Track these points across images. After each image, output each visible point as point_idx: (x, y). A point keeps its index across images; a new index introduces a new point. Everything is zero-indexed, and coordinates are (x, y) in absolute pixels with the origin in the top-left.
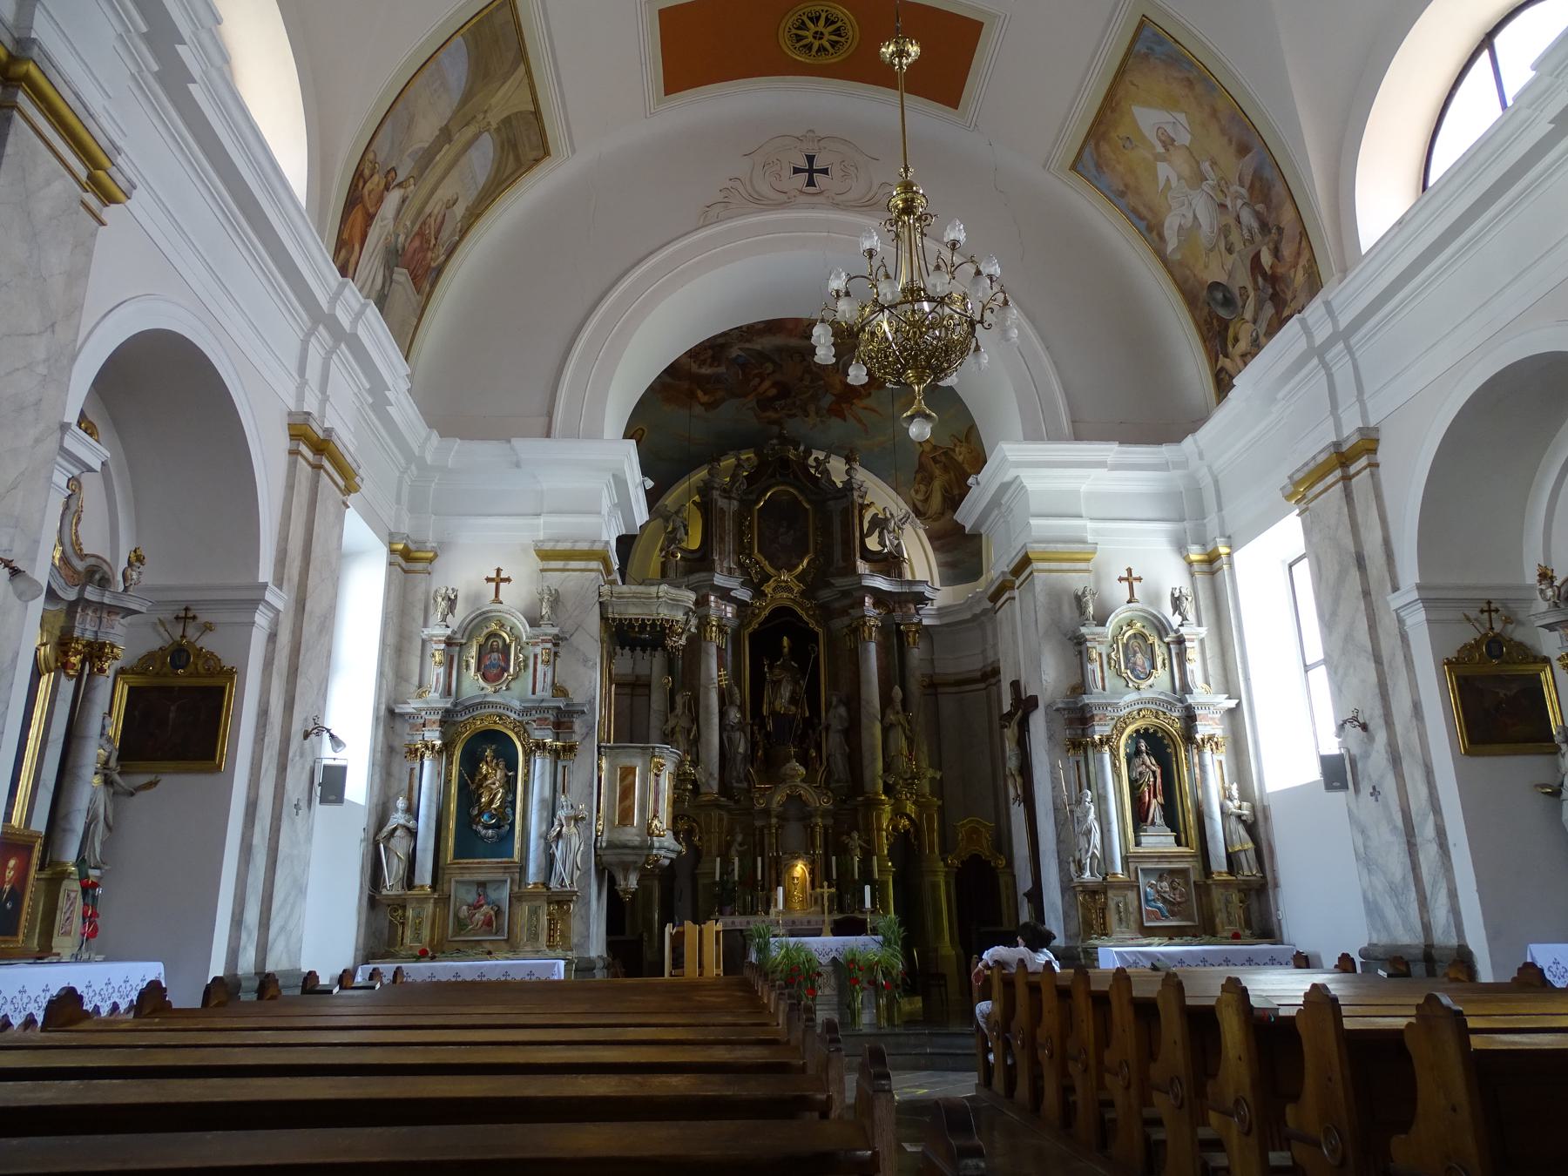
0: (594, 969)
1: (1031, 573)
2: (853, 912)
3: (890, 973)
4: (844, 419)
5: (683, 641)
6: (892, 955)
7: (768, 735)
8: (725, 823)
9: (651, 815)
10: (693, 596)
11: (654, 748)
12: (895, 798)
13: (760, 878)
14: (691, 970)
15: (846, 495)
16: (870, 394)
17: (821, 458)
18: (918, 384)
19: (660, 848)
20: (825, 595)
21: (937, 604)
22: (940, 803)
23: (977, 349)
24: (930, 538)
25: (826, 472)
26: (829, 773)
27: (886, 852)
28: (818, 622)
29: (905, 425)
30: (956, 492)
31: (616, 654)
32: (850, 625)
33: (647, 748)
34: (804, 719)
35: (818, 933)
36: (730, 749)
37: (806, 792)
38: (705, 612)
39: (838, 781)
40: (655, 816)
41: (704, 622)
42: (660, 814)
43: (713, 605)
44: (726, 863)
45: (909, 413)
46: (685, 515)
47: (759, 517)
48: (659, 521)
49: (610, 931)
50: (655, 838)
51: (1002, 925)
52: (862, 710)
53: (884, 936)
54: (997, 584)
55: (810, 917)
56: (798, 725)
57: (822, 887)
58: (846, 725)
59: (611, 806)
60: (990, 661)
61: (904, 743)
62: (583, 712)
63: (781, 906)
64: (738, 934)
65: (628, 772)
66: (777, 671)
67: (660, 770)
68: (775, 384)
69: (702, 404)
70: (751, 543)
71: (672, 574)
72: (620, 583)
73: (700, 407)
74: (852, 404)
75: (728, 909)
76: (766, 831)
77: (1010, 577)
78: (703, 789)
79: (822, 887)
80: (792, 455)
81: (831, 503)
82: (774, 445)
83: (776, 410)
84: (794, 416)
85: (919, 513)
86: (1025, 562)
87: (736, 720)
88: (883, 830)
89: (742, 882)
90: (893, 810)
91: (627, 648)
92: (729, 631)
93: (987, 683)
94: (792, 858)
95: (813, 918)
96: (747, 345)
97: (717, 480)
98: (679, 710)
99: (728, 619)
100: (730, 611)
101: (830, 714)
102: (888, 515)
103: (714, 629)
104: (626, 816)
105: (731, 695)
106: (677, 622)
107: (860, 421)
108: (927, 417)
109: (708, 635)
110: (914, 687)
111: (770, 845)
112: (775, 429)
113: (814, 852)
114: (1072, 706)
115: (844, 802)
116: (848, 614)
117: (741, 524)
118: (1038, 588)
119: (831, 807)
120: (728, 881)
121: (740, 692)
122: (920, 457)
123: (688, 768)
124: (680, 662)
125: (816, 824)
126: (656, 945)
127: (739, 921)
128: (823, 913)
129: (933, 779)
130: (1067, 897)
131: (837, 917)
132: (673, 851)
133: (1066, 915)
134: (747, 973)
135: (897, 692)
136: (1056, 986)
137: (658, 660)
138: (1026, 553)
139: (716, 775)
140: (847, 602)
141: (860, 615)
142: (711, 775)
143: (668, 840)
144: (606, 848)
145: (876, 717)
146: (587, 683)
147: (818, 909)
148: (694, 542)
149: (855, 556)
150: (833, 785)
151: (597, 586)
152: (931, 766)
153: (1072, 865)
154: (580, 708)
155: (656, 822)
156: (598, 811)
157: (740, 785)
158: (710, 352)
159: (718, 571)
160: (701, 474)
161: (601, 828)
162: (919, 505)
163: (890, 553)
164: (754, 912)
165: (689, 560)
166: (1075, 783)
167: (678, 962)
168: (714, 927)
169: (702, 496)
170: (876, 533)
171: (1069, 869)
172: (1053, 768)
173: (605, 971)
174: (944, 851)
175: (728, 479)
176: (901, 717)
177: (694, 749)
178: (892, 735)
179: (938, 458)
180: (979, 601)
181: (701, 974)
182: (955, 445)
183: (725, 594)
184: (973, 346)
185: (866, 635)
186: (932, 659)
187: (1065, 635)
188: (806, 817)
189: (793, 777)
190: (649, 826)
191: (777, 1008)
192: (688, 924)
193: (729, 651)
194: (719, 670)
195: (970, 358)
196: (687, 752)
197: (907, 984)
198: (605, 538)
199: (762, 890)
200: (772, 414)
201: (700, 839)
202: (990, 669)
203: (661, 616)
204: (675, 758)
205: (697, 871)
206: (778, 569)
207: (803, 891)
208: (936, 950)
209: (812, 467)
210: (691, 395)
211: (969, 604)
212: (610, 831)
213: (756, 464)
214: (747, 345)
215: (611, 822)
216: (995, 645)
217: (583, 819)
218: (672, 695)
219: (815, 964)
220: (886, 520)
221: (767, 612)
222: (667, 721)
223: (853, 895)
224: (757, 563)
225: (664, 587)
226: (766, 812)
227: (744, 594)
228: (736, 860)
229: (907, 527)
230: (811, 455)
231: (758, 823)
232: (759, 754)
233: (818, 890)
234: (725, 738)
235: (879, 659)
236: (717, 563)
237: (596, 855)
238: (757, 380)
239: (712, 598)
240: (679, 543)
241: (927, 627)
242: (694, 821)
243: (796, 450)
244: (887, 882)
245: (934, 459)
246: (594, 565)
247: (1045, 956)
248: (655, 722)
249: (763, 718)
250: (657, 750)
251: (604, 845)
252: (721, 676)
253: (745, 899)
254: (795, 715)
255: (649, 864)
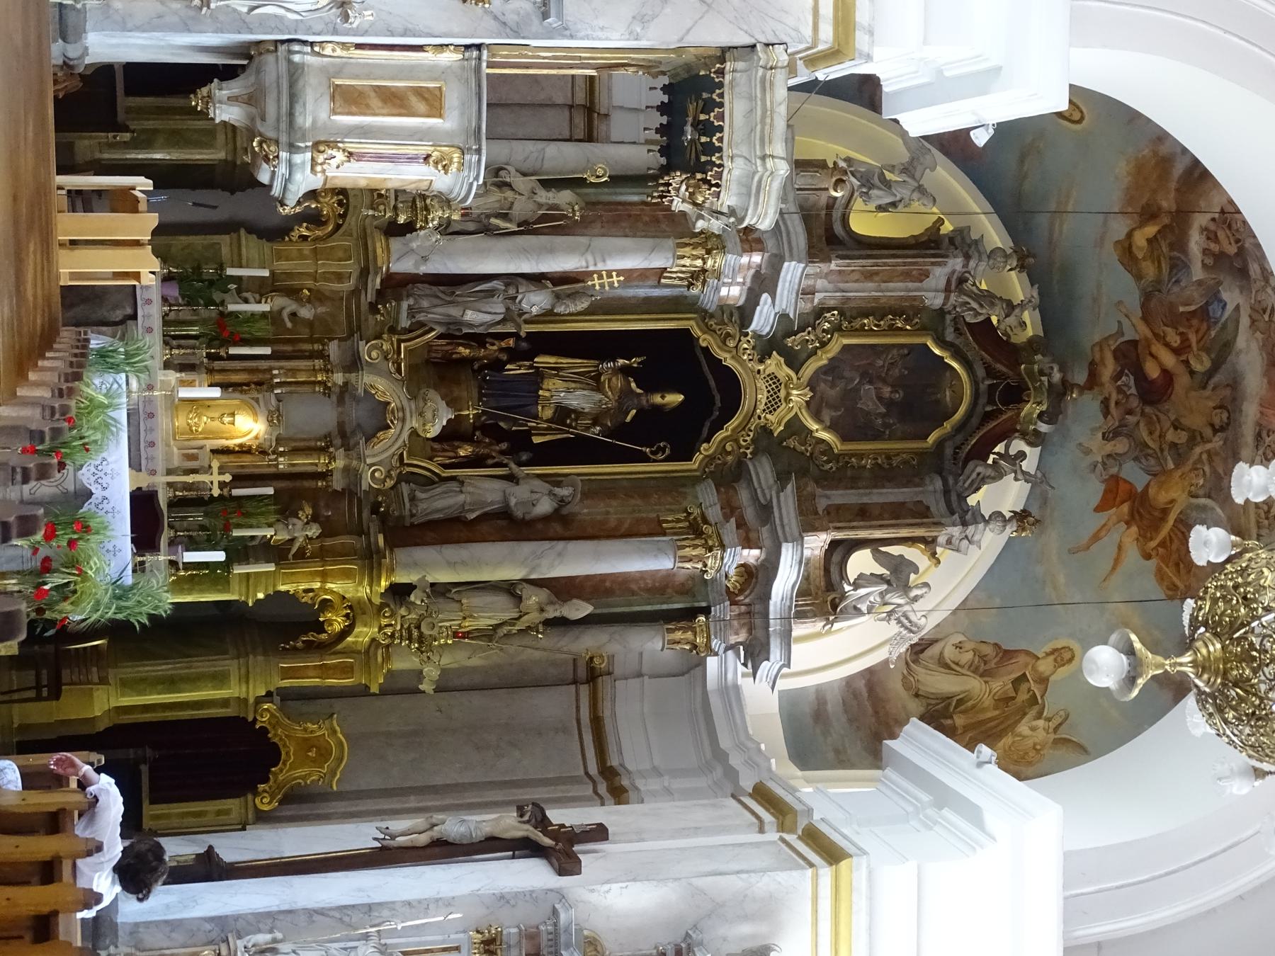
0: (64, 40)
1: (811, 865)
2: (171, 526)
3: (65, 599)
4: (1099, 509)
5: (678, 205)
6: (98, 603)
7: (497, 365)
8: (336, 286)
9: (352, 147)
10: (765, 224)
11: (479, 151)
12: (382, 606)
13: (233, 351)
14: (69, 225)
15: (952, 513)
16: (1147, 557)
17: (1025, 465)
18: (1194, 663)
19: (291, 165)
20: (763, 472)
21: (746, 684)
22: (374, 689)
23: (1259, 774)
24: (870, 672)
25: (998, 474)
26: (428, 482)
27: (283, 588)
28: (711, 458)
29: (1114, 637)
30: (959, 721)
31: (655, 76)
32: (706, 521)
33: (478, 140)
34: (528, 434)
35: (135, 464)
36: (470, 295)
37: (390, 443)
38: (729, 245)
39: (413, 499)
40: (351, 154)
41: (711, 243)
42: (354, 165)
43: (745, 260)
44: (263, 288)
45: (1138, 645)
46: (916, 206)
47: (911, 347)
48: (904, 156)
49: (132, 69)
50: (308, 155)
51: (152, 802)
52: (547, 544)
53: (132, 588)
54: (789, 799)
55: (160, 445)
56: (515, 422)
57: (222, 471)
58: (519, 513)
59: (370, 71)
60: (640, 783)
61: (484, 622)
62: (545, 15)
63: (185, 393)
64: (129, 311)
65: (433, 102)
66: (618, 382)
67: (436, 163)
68: (1167, 375)
69: (1130, 235)
70: (861, 331)
71: (804, 180)
72: (792, 82)
73: (1125, 231)
74: (1127, 523)
75: (174, 291)
76: (318, 363)
77: (802, 824)
78: (396, 243)
79: (222, 471)
80: (1031, 409)
81: (939, 484)
82: (1049, 375)
83: (1117, 377)
84: (1106, 412)
85: (918, 650)
86: (832, 854)
87: (525, 306)
88: (324, 582)
89: (225, 317)
90: (359, 601)
91: (666, 99)
92: (695, 291)
93: (599, 779)
94: (270, 413)
95: (159, 452)
96: (1245, 321)
97: (983, 265)
98: (545, 196)
99: (717, 289)
100: (733, 292)
101: (537, 483)
102: (914, 593)
103: (699, 263)
104: (349, 99)
105: (572, 296)
106: (718, 195)
107: (1096, 537)
108: (1131, 680)
109: (687, 251)
110: (589, 642)
111: (294, 371)
112: (1080, 377)
113: (282, 454)
114: (563, 939)
115: (375, 509)
116: (727, 518)
117: (897, 312)
118: (783, 877)
119: (364, 487)
120: (227, 291)
121: (579, 314)
122: (1027, 653)
123: (437, 215)
124: (635, 198)
125: (333, 458)
126: (106, 156)
127: (151, 313)
128: (169, 472)
129: (419, 675)
130: (208, 926)
131: (163, 500)
132: (285, 189)
133: (174, 925)
134: (67, 335)
135: (579, 609)
136: (55, 914)
137: (643, 157)
138: (851, 856)
139: (424, 269)
140: (750, 514)
141: (726, 542)
142: (425, 259)
143: (305, 181)
144: (290, 62)
145: (533, 570)
146: (601, 22)
147: (176, 462)
148: (864, 223)
149: (838, 529)
150: (405, 489)
151: (785, 39)
152: (444, 672)
153: (268, 937)
154: (553, 11)
155: (340, 156)
156: (359, 46)
157: (404, 314)
158: (1232, 250)
159: (810, 270)
160: (994, 235)
161: (328, 51)
162: (934, 651)
163: (843, 596)
164: (168, 340)
165: (829, 216)
166: (419, 944)
167: (82, 201)
168: (148, 268)
169: (951, 239)
170: (880, 570)
171: (259, 931)
172: (448, 903)
173: (60, 62)
174: (287, 697)
175: (984, 287)
176: (534, 617)
177: (471, 226)
178: (502, 600)
179: (1024, 687)
180: (751, 764)
181: (62, 245)
182: (1049, 720)
183: (764, 283)
184: (1266, 766)
185: (688, 552)
186: (640, 675)
187: (695, 927)
188: (344, 437)
189: (421, 414)
190: (331, 144)
191: (26, 402)
192: (153, 220)
193: (657, 292)
194: (620, 272)
195: (1242, 759)
196: (466, 213)
197: (44, 630)
198: (877, 53)
199: (209, 356)
200: (1109, 369)
201: (304, 238)
202: (625, 782)
203: (727, 163)
204: (458, 192)
205: (243, 232)
206: (812, 384)
207: (210, 435)
208: (103, 681)
209: (1007, 447)
210: (1148, 214)
211: (747, 744)
212: (323, 69)
213: (1014, 340)
214: (1245, 321)
215: (339, 72)
216: (668, 793)
217: (346, 17)
218: (575, 183)
219: (79, 458)
220: (906, 588)
221: (729, 362)
222: (524, 174)
223: (202, 528)
224: (824, 344)
225: (783, 169)
226: (354, 364)
227: (763, 320)
228: (264, 307)
229: (893, 628)
230: (1031, 444)
231: (333, 349)
232: (461, 349)
233: (215, 465)
234: (496, 284)
235: (642, 575)
236: (824, 267)
237: (276, 43)
238: (1175, 340)
239: (757, 258)
240: (862, 194)
241: (702, 664)
242: (338, 227)
243: (1040, 416)
244: (228, 591)
245: (1023, 678)
246: (827, 34)
247: (105, 884)
248: (522, 152)
249: (530, 355)
250: (475, 158)
251: (297, 58)
252: (609, 275)
253: (191, 323)
254: (536, 417)
255: (260, 144)
